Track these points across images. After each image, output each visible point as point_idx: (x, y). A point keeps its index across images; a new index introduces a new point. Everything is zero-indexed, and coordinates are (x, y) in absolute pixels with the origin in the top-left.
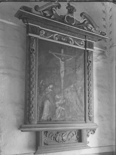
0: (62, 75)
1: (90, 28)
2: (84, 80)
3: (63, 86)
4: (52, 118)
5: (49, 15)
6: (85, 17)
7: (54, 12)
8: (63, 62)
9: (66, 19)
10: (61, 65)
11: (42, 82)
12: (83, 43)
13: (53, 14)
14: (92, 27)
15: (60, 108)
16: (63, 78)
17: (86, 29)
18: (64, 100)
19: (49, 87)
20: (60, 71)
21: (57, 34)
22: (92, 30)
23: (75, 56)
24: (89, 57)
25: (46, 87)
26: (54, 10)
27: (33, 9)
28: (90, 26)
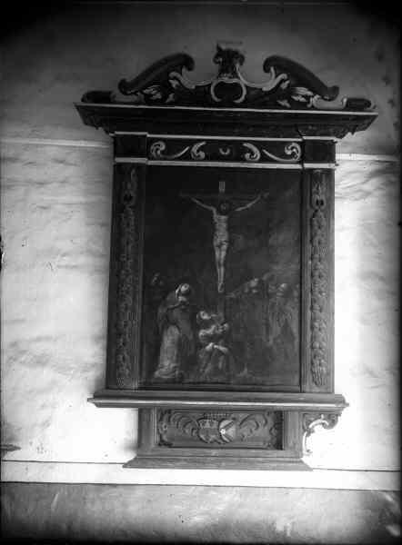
0: (221, 255)
1: (302, 99)
2: (297, 260)
3: (222, 286)
4: (186, 375)
5: (159, 96)
6: (279, 70)
7: (174, 83)
8: (223, 218)
9: (212, 93)
10: (217, 227)
11: (158, 278)
12: (294, 150)
13: (172, 90)
14: (310, 93)
15: (213, 347)
16: (222, 262)
17: (288, 105)
18: (226, 325)
19: (177, 291)
20: (215, 244)
21: (203, 143)
22: (309, 102)
23: (266, 195)
24: (314, 189)
25: (169, 289)
26: (175, 78)
27: (116, 91)
28: (303, 91)
